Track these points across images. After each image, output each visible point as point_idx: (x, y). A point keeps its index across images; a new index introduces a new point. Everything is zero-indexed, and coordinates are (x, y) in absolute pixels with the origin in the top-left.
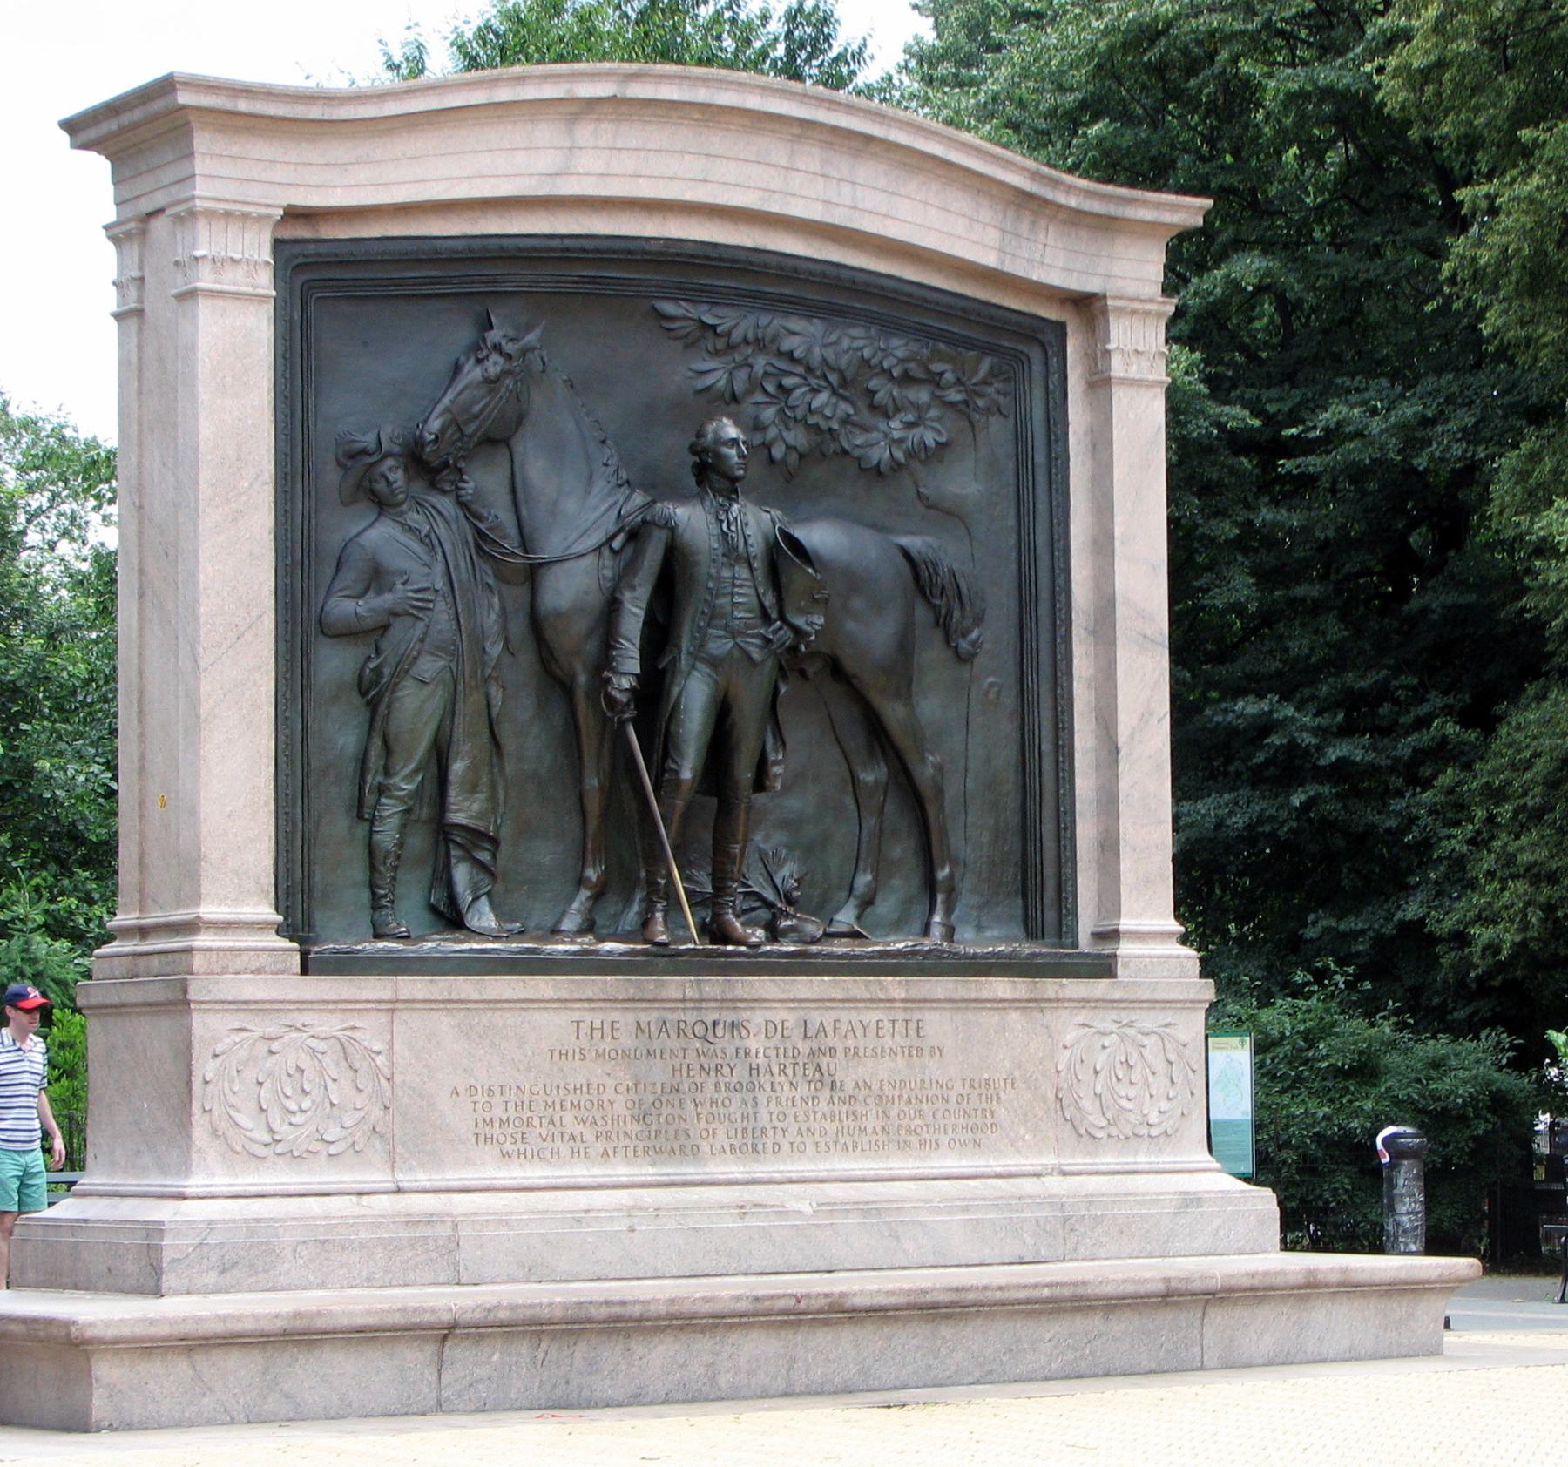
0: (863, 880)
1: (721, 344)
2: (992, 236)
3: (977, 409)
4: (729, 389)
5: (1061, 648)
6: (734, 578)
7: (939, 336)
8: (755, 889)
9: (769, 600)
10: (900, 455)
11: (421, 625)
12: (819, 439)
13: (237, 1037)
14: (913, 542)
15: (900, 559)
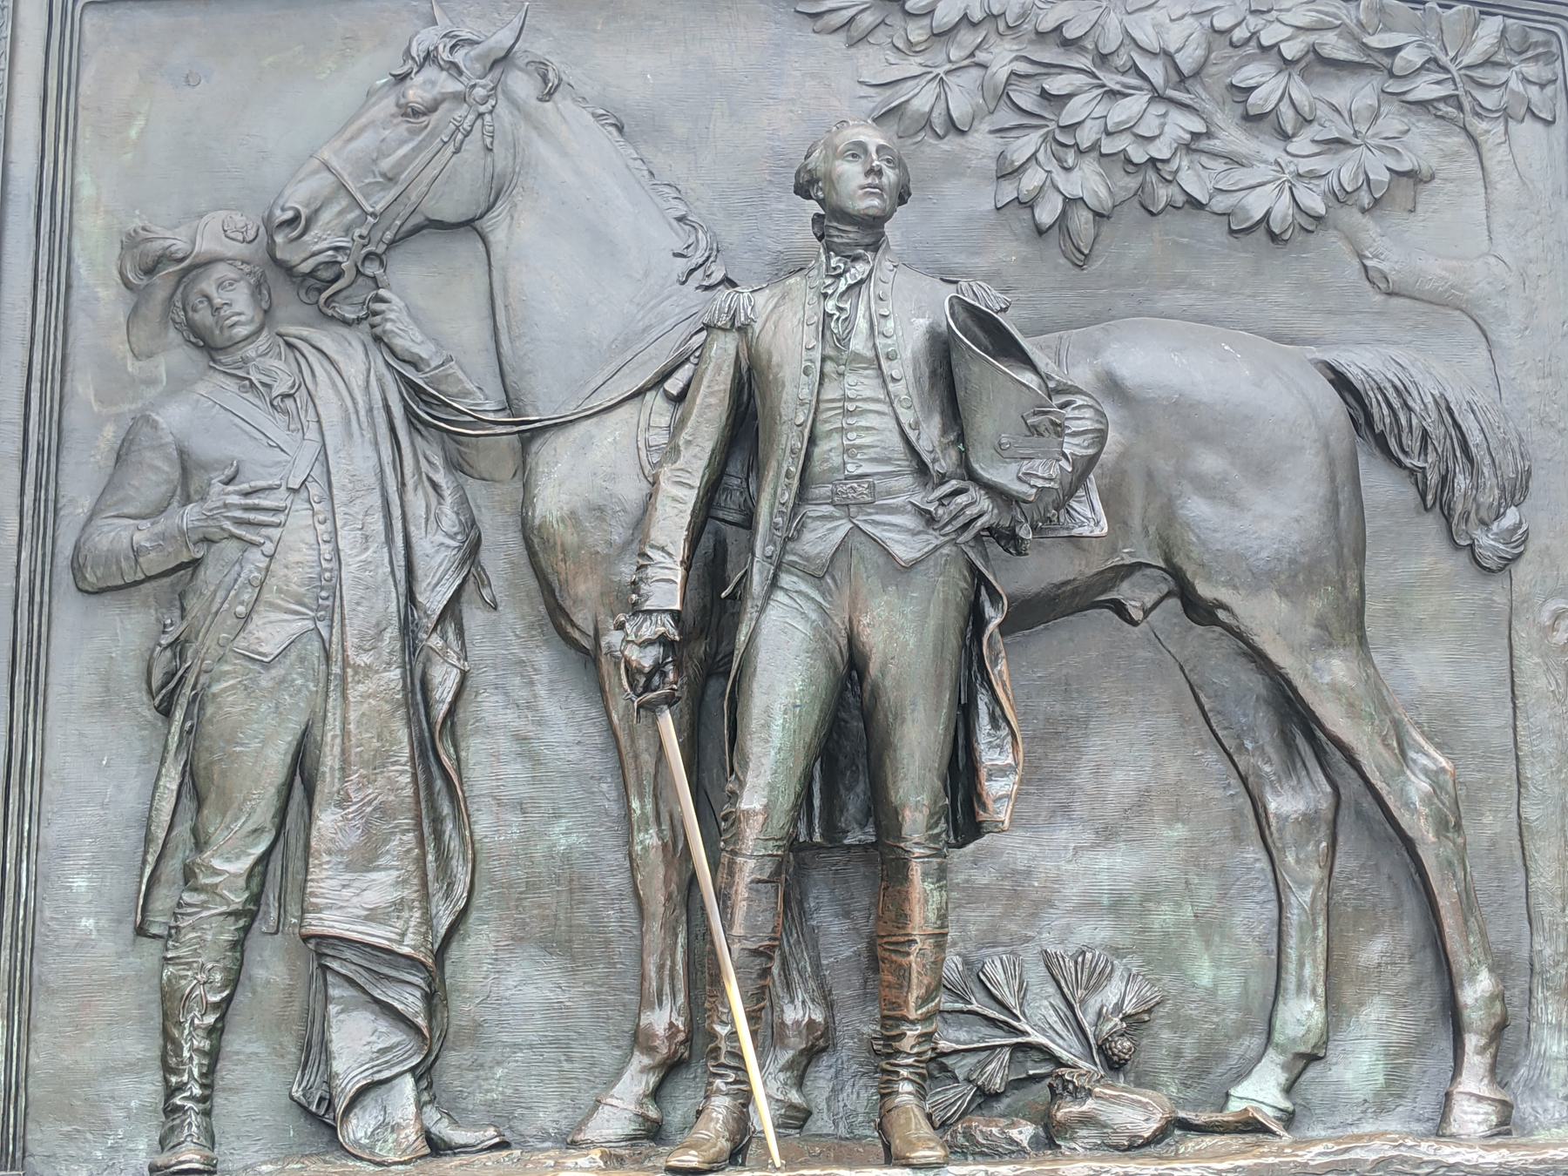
0: (1301, 1014)
1: (917, 32)
3: (1480, 112)
4: (939, 110)
6: (845, 398)
8: (1036, 1038)
9: (929, 437)
10: (1317, 205)
12: (1133, 183)
14: (1359, 362)
15: (1330, 403)
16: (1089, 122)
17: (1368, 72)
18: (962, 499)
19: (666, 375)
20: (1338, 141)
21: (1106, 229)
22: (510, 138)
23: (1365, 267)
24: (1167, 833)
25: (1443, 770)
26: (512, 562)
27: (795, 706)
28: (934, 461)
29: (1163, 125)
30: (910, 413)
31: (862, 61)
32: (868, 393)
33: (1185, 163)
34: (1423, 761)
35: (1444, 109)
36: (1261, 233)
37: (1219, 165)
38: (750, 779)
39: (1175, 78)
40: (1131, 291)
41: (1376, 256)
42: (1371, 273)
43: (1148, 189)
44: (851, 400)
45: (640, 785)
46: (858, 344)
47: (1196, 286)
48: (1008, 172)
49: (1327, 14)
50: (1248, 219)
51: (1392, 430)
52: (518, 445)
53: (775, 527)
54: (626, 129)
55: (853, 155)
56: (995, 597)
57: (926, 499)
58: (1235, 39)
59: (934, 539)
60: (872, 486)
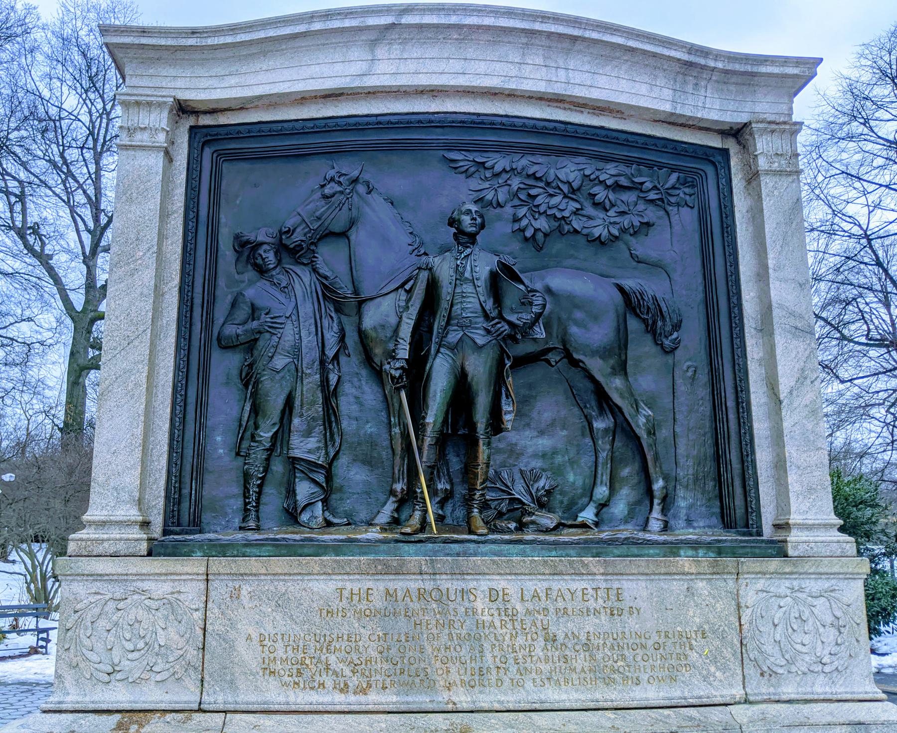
1: (488, 174)
2: (667, 93)
5: (737, 341)
6: (463, 292)
7: (640, 162)
8: (517, 496)
9: (489, 305)
10: (616, 232)
11: (275, 338)
13: (92, 599)
14: (629, 284)
18: (499, 326)
37: (585, 219)
38: (429, 412)
46: (467, 275)
47: (576, 258)
48: (516, 220)
59: (490, 338)
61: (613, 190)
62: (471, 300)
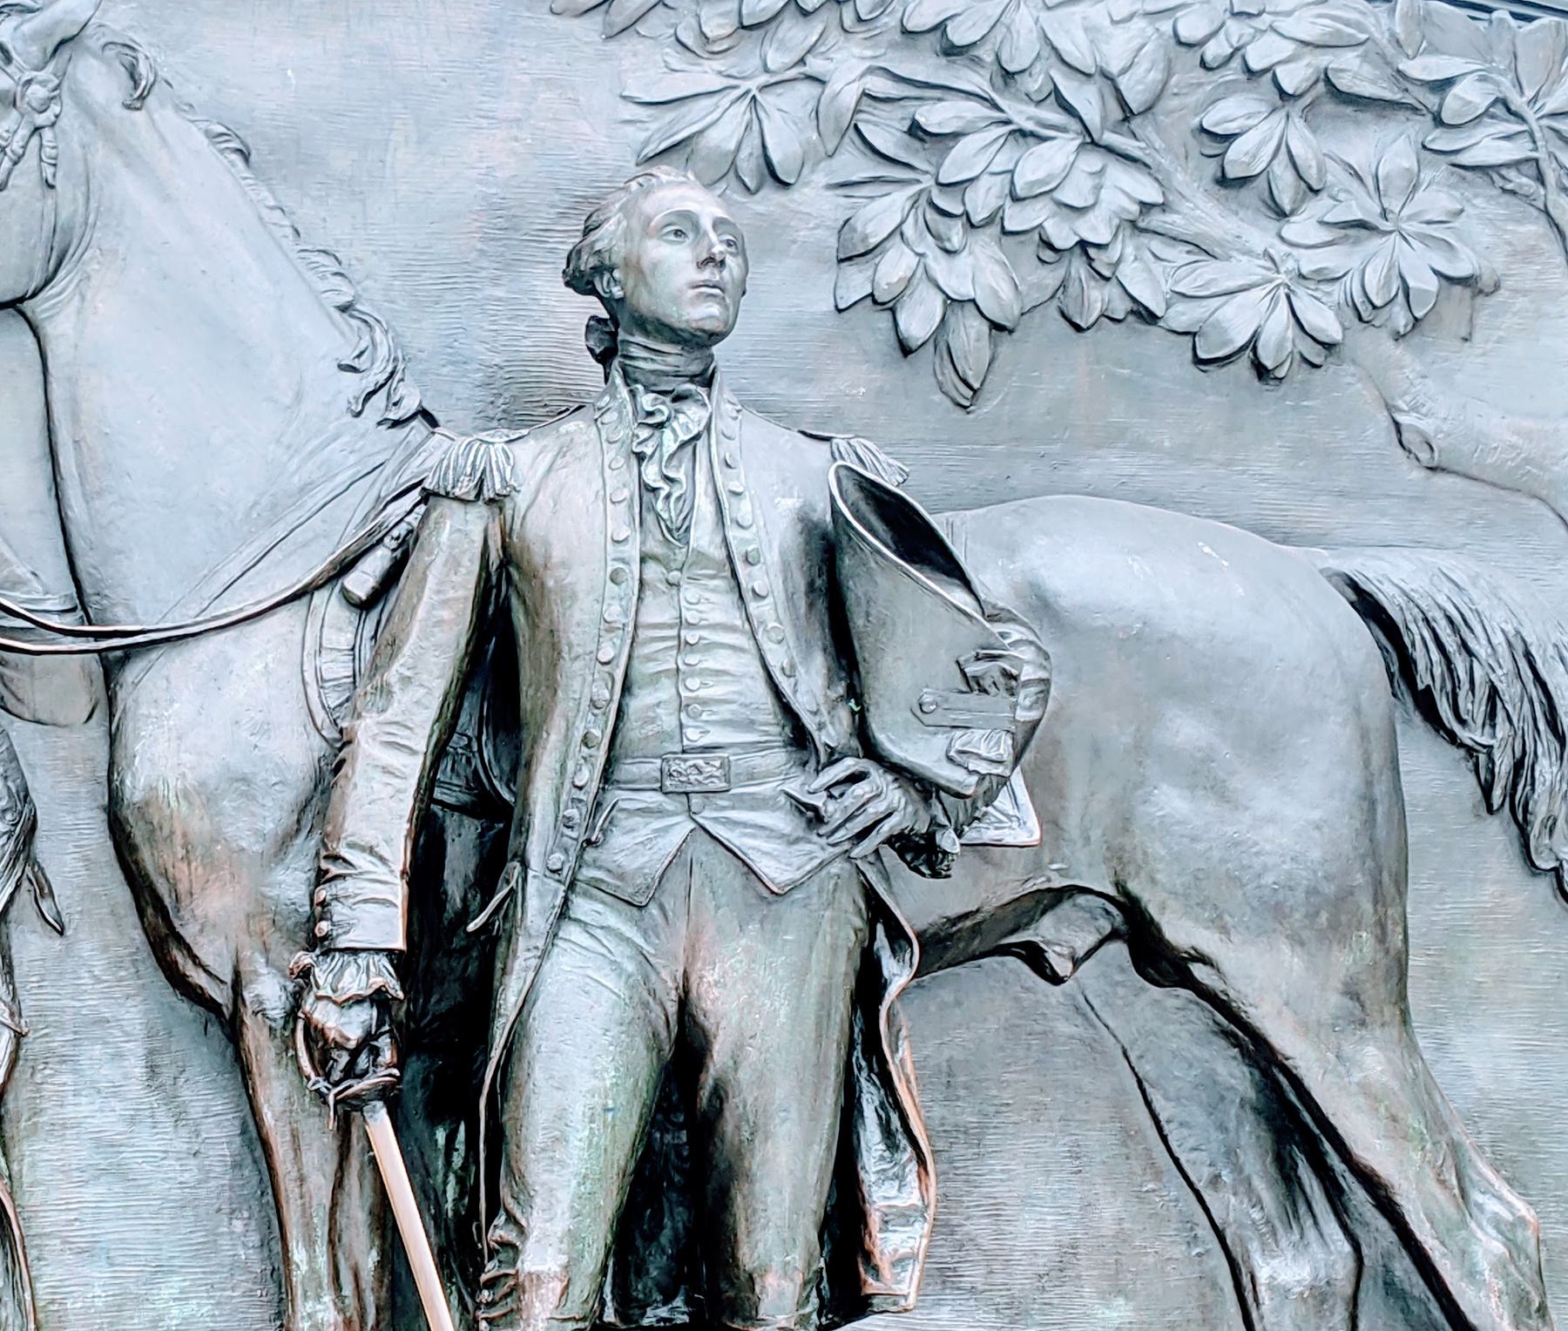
4: (752, 145)
6: (681, 623)
9: (812, 688)
10: (1326, 323)
12: (1050, 278)
14: (1396, 578)
16: (985, 177)
17: (1402, 115)
18: (861, 789)
19: (345, 566)
20: (1362, 225)
21: (1006, 345)
22: (80, 168)
23: (1397, 425)
24: (1101, 1312)
25: (1522, 1221)
26: (86, 859)
27: (607, 1110)
28: (821, 726)
29: (1098, 188)
30: (782, 649)
31: (626, 64)
32: (717, 617)
33: (1130, 250)
34: (1492, 1206)
35: (1519, 180)
36: (1243, 366)
37: (1179, 254)
38: (535, 1221)
39: (1119, 115)
40: (1042, 449)
41: (1415, 409)
42: (1406, 436)
43: (1073, 289)
44: (691, 626)
45: (308, 1225)
46: (703, 536)
47: (1140, 446)
49: (1348, 23)
50: (1225, 344)
51: (1443, 687)
52: (98, 670)
53: (568, 823)
54: (253, 158)
55: (677, 233)
56: (897, 935)
57: (809, 786)
58: (1208, 58)
59: (816, 849)
60: (725, 765)
61: (1309, 112)
62: (720, 660)
